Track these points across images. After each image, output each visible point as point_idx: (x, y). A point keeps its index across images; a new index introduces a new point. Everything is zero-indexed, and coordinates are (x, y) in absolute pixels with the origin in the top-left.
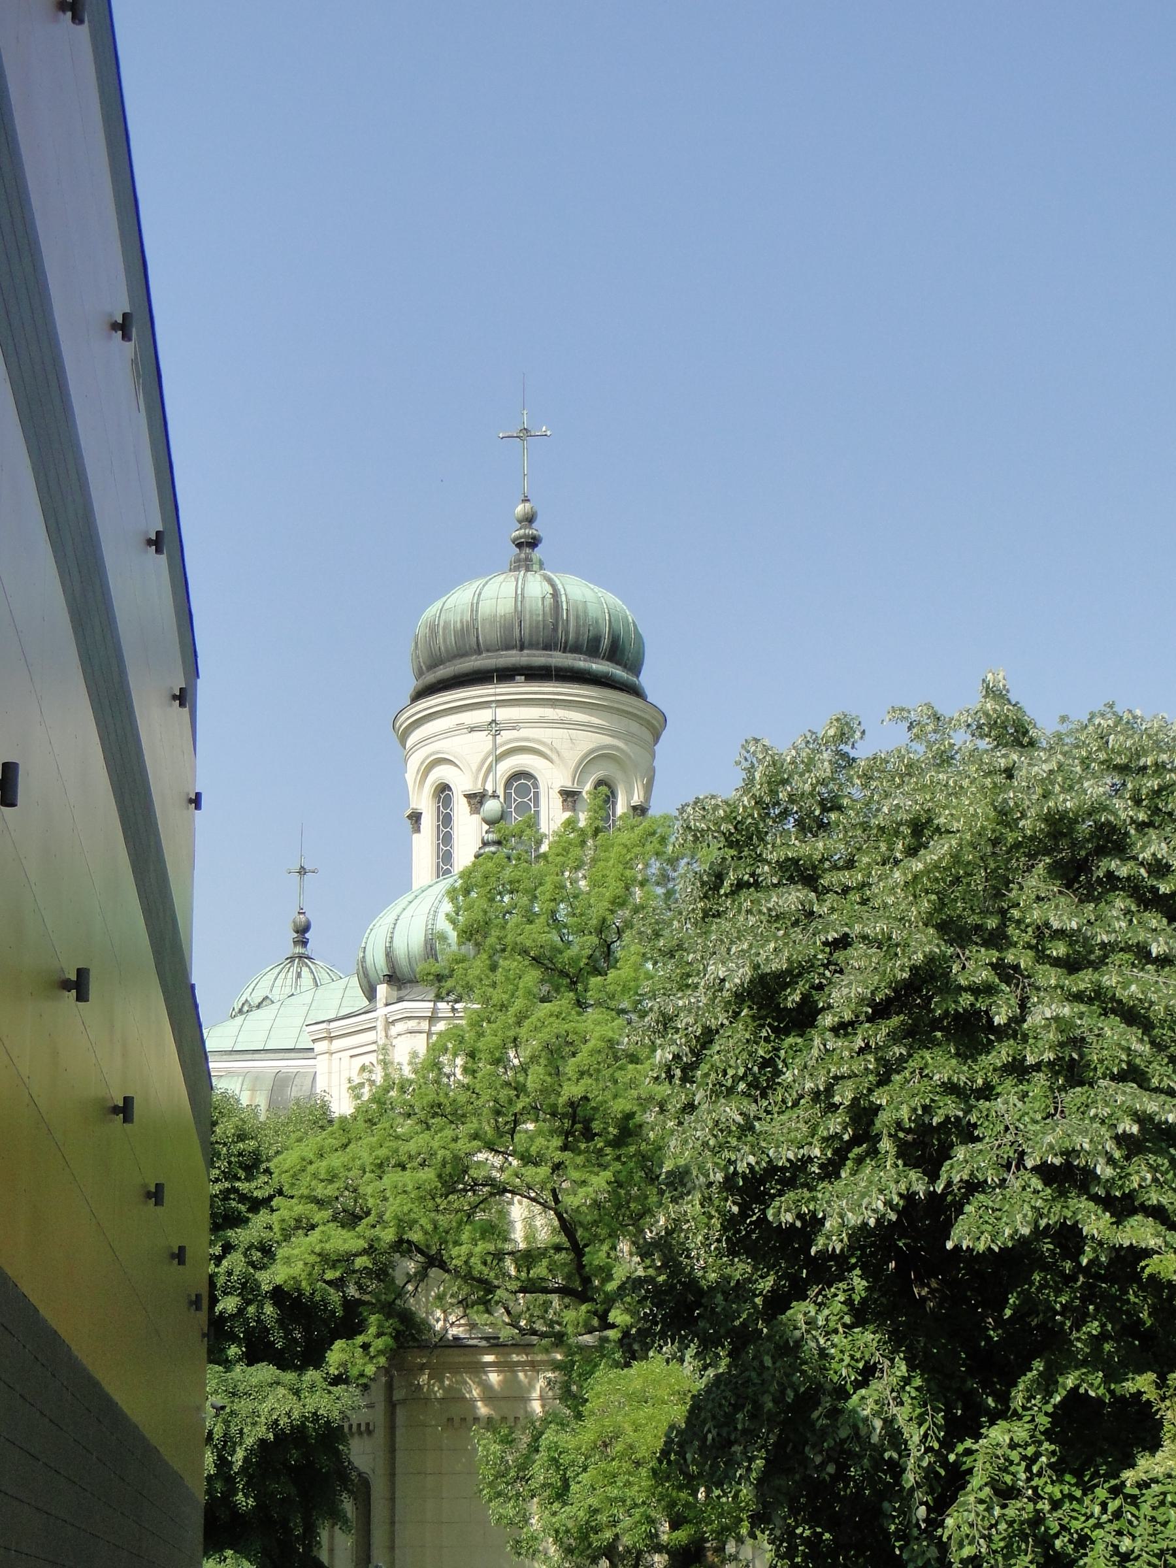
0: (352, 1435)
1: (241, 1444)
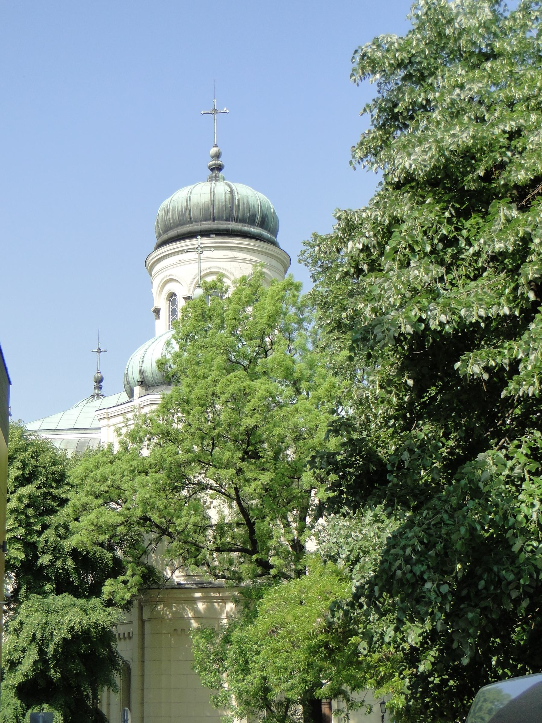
0: (120, 639)
1: (52, 641)
